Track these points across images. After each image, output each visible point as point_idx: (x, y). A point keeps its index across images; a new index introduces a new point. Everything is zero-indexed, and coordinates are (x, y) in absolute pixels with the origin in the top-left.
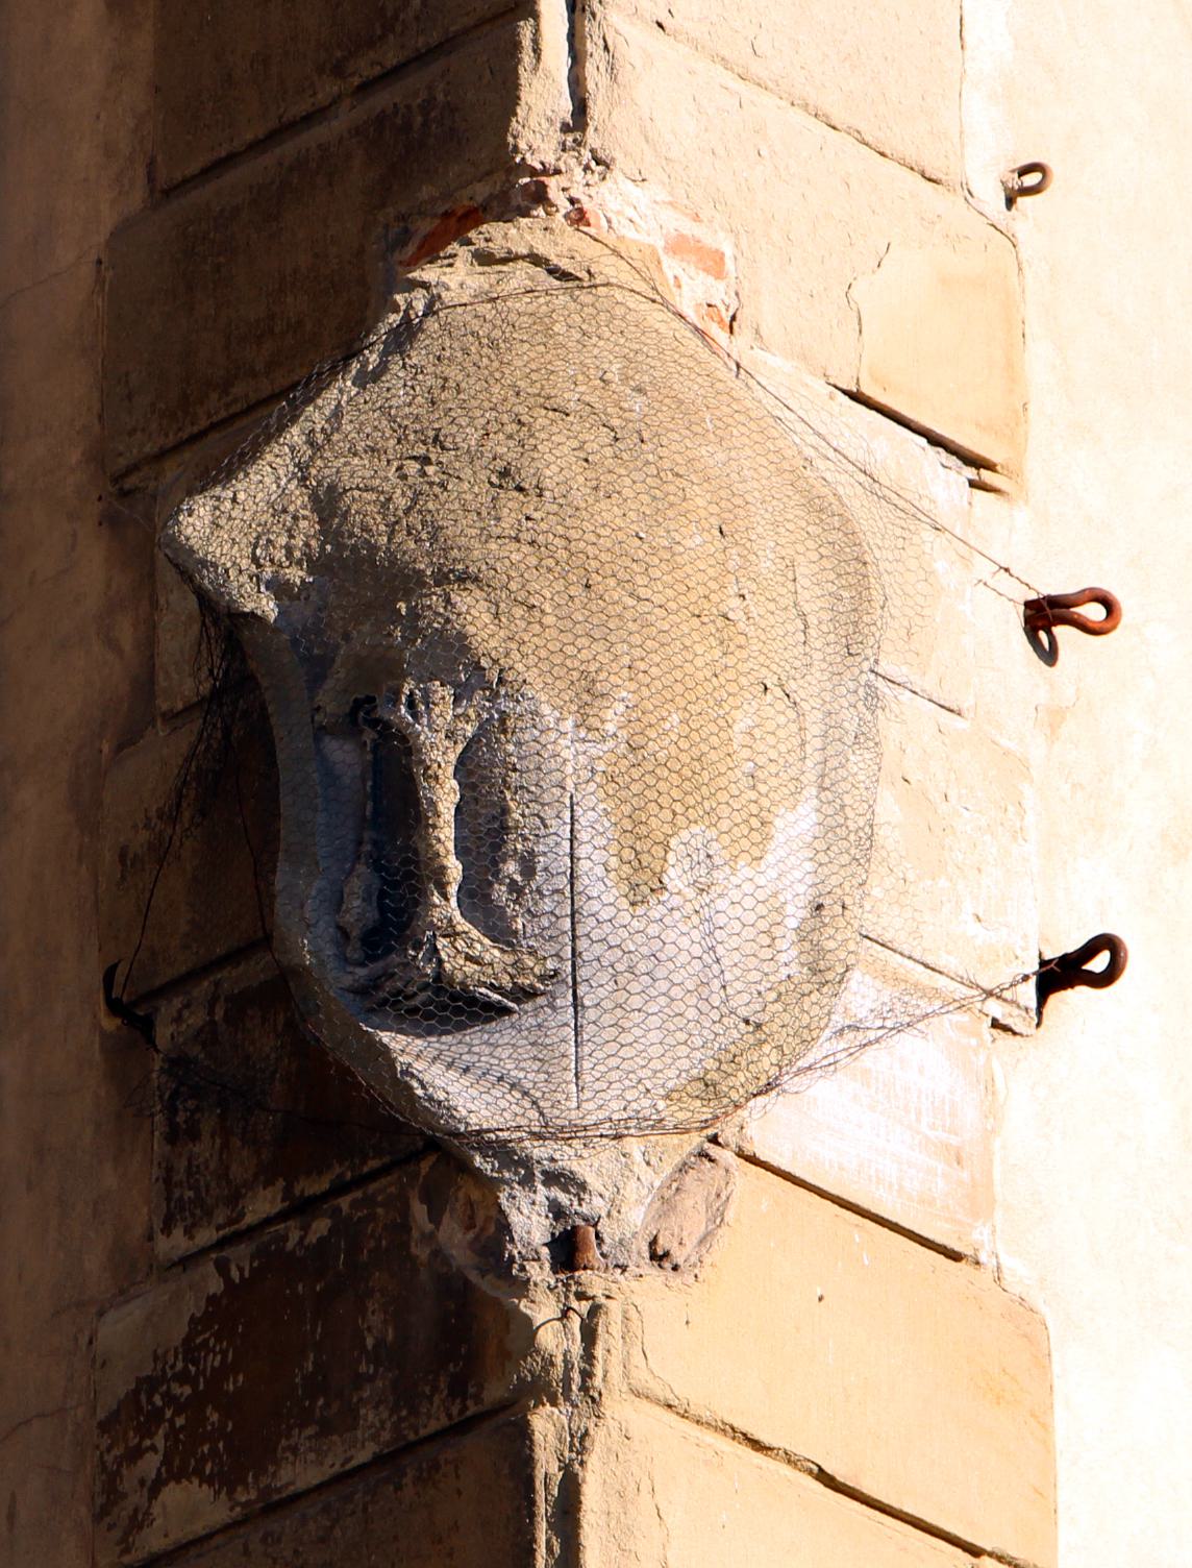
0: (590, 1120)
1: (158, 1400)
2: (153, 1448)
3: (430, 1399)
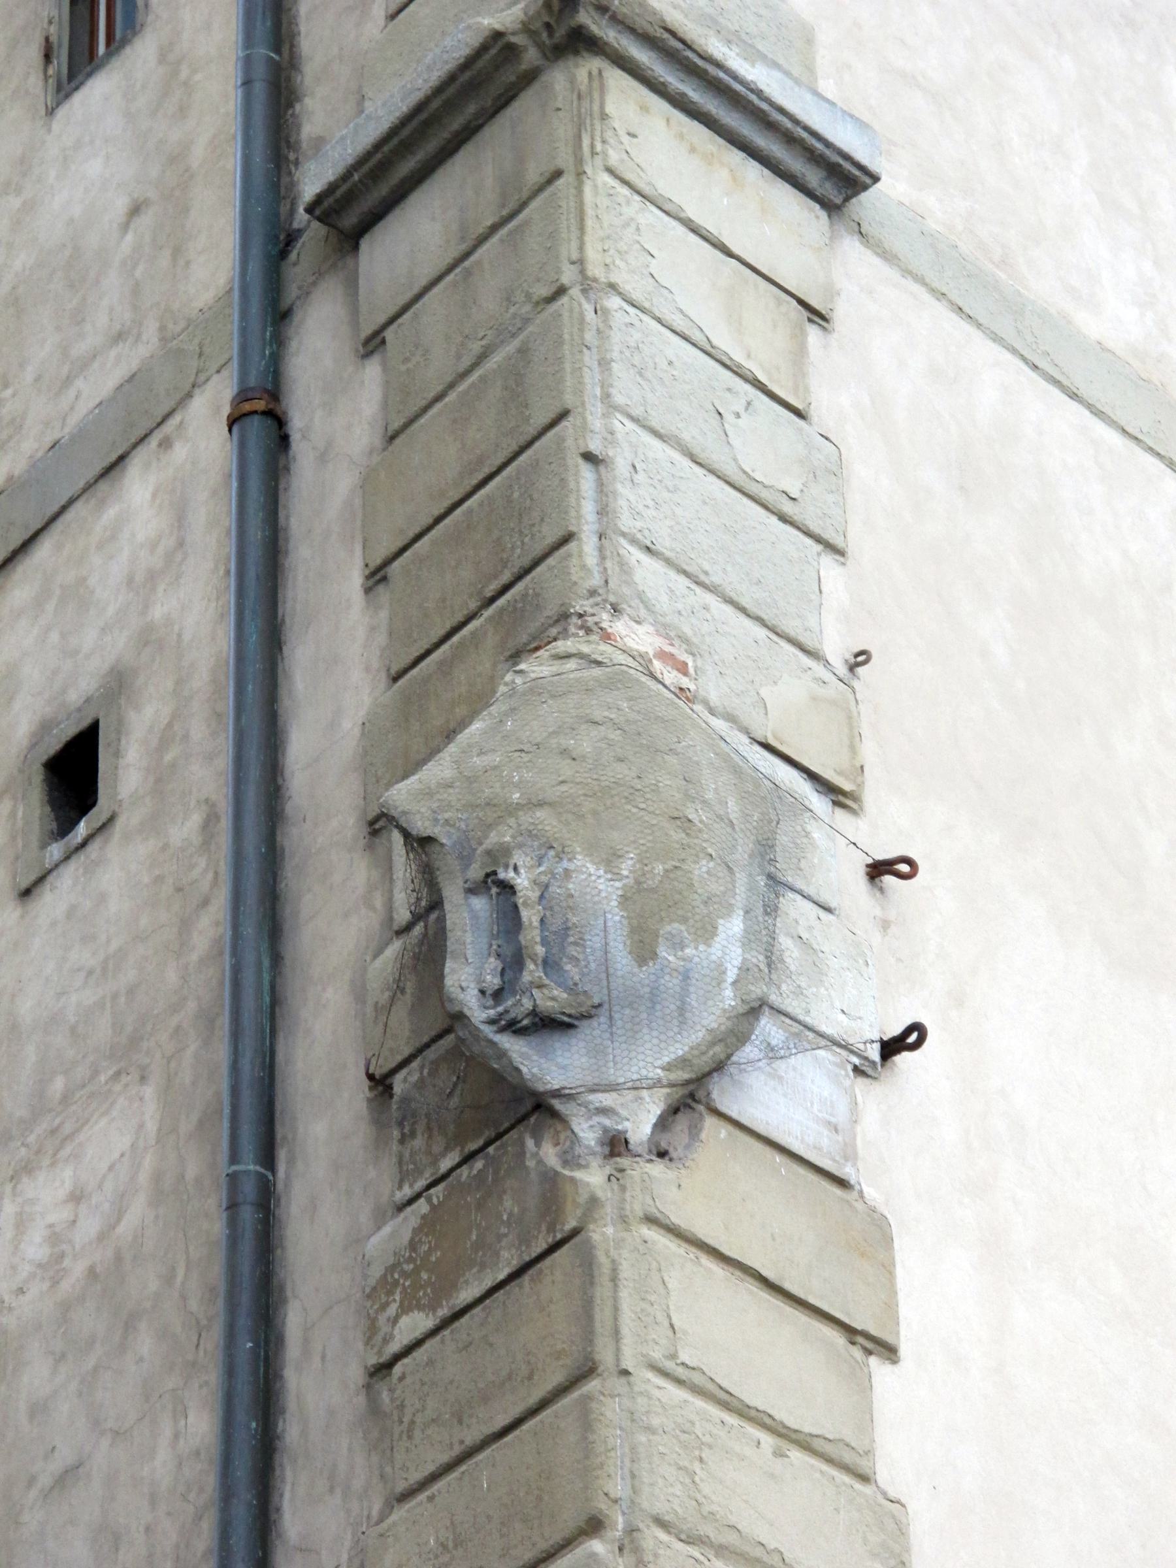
0: (621, 1080)
1: (396, 1276)
2: (395, 1300)
3: (537, 1238)
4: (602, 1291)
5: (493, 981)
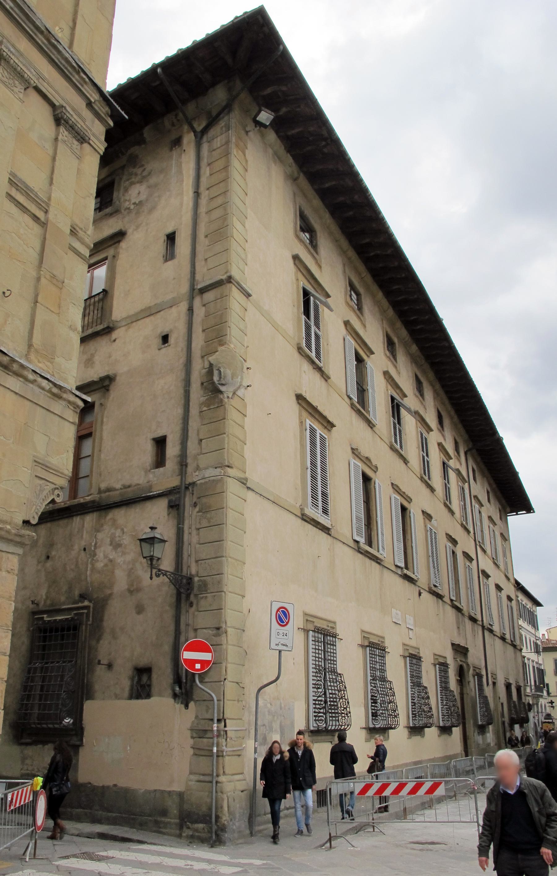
4: (226, 411)
5: (218, 379)
